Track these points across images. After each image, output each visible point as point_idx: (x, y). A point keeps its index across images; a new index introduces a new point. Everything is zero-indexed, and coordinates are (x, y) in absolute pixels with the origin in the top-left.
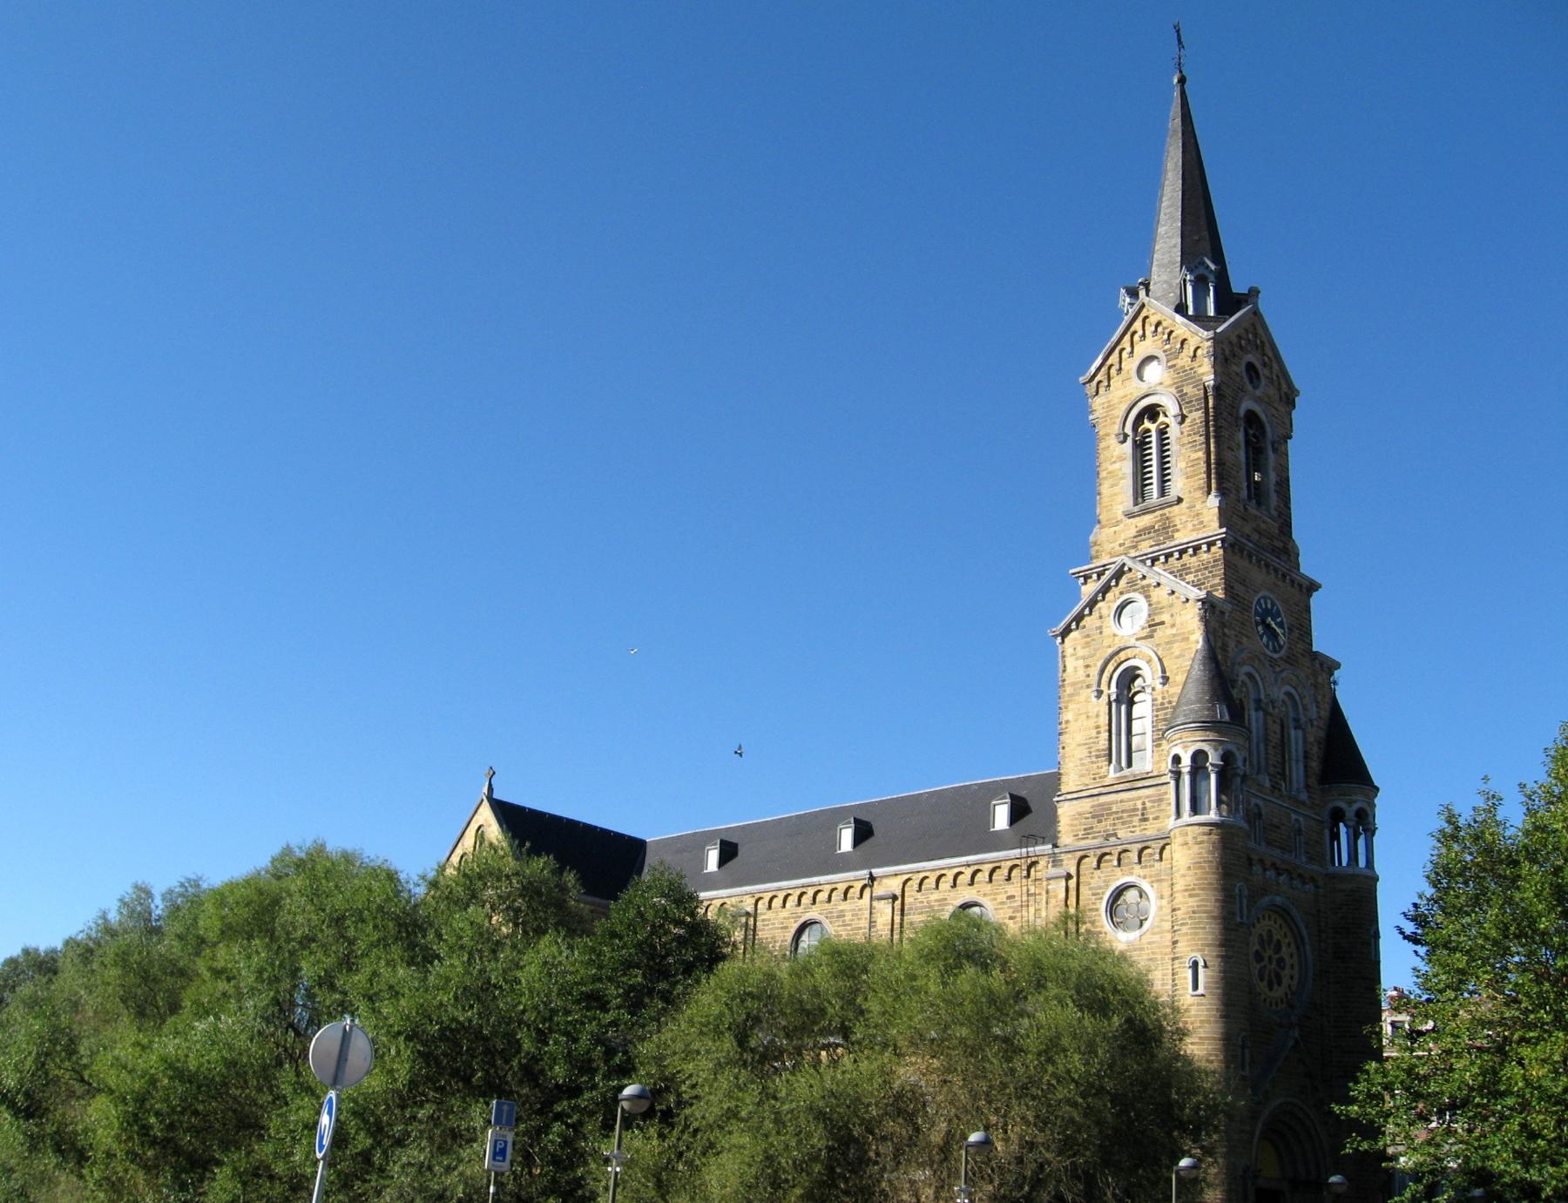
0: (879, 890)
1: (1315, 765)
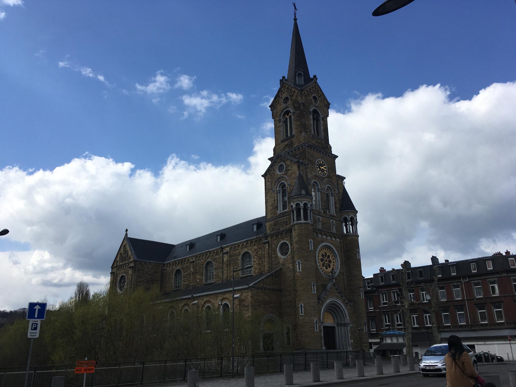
1: (338, 206)
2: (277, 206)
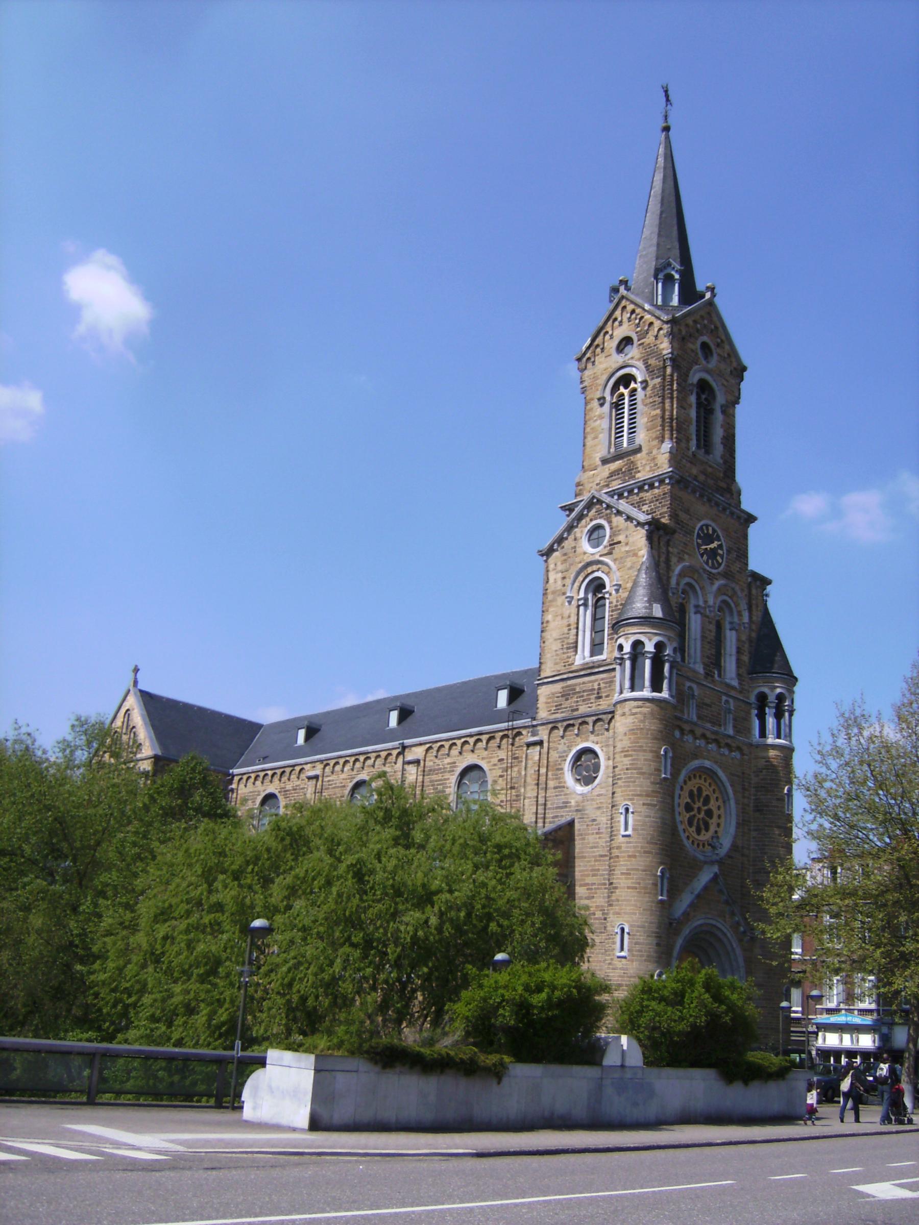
0: (409, 756)
1: (745, 658)
2: (577, 642)
